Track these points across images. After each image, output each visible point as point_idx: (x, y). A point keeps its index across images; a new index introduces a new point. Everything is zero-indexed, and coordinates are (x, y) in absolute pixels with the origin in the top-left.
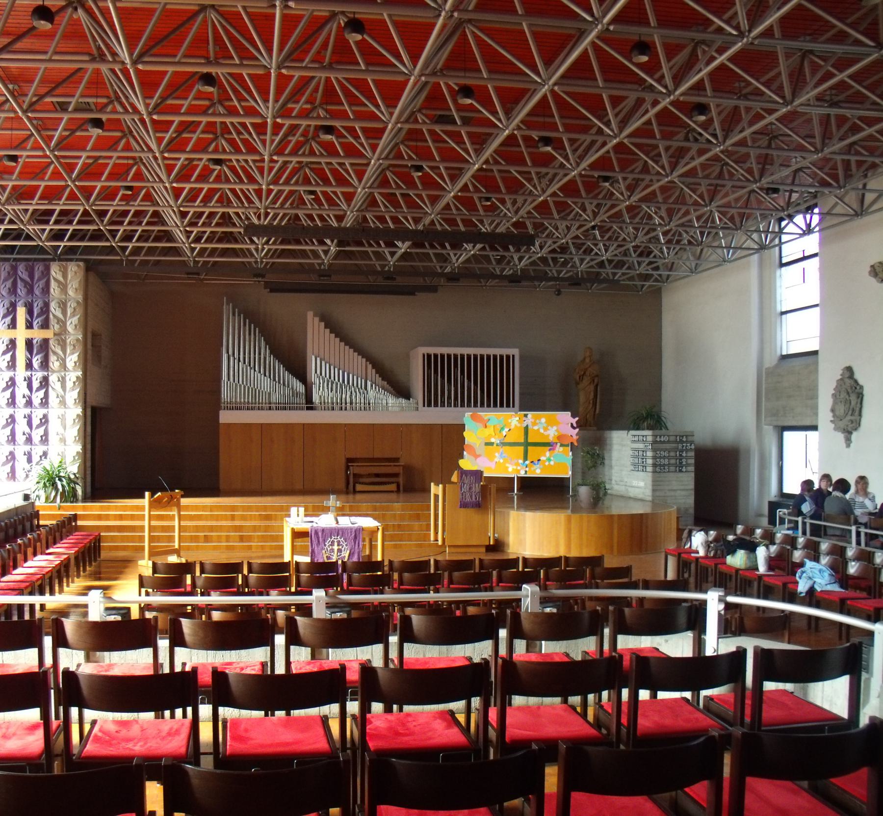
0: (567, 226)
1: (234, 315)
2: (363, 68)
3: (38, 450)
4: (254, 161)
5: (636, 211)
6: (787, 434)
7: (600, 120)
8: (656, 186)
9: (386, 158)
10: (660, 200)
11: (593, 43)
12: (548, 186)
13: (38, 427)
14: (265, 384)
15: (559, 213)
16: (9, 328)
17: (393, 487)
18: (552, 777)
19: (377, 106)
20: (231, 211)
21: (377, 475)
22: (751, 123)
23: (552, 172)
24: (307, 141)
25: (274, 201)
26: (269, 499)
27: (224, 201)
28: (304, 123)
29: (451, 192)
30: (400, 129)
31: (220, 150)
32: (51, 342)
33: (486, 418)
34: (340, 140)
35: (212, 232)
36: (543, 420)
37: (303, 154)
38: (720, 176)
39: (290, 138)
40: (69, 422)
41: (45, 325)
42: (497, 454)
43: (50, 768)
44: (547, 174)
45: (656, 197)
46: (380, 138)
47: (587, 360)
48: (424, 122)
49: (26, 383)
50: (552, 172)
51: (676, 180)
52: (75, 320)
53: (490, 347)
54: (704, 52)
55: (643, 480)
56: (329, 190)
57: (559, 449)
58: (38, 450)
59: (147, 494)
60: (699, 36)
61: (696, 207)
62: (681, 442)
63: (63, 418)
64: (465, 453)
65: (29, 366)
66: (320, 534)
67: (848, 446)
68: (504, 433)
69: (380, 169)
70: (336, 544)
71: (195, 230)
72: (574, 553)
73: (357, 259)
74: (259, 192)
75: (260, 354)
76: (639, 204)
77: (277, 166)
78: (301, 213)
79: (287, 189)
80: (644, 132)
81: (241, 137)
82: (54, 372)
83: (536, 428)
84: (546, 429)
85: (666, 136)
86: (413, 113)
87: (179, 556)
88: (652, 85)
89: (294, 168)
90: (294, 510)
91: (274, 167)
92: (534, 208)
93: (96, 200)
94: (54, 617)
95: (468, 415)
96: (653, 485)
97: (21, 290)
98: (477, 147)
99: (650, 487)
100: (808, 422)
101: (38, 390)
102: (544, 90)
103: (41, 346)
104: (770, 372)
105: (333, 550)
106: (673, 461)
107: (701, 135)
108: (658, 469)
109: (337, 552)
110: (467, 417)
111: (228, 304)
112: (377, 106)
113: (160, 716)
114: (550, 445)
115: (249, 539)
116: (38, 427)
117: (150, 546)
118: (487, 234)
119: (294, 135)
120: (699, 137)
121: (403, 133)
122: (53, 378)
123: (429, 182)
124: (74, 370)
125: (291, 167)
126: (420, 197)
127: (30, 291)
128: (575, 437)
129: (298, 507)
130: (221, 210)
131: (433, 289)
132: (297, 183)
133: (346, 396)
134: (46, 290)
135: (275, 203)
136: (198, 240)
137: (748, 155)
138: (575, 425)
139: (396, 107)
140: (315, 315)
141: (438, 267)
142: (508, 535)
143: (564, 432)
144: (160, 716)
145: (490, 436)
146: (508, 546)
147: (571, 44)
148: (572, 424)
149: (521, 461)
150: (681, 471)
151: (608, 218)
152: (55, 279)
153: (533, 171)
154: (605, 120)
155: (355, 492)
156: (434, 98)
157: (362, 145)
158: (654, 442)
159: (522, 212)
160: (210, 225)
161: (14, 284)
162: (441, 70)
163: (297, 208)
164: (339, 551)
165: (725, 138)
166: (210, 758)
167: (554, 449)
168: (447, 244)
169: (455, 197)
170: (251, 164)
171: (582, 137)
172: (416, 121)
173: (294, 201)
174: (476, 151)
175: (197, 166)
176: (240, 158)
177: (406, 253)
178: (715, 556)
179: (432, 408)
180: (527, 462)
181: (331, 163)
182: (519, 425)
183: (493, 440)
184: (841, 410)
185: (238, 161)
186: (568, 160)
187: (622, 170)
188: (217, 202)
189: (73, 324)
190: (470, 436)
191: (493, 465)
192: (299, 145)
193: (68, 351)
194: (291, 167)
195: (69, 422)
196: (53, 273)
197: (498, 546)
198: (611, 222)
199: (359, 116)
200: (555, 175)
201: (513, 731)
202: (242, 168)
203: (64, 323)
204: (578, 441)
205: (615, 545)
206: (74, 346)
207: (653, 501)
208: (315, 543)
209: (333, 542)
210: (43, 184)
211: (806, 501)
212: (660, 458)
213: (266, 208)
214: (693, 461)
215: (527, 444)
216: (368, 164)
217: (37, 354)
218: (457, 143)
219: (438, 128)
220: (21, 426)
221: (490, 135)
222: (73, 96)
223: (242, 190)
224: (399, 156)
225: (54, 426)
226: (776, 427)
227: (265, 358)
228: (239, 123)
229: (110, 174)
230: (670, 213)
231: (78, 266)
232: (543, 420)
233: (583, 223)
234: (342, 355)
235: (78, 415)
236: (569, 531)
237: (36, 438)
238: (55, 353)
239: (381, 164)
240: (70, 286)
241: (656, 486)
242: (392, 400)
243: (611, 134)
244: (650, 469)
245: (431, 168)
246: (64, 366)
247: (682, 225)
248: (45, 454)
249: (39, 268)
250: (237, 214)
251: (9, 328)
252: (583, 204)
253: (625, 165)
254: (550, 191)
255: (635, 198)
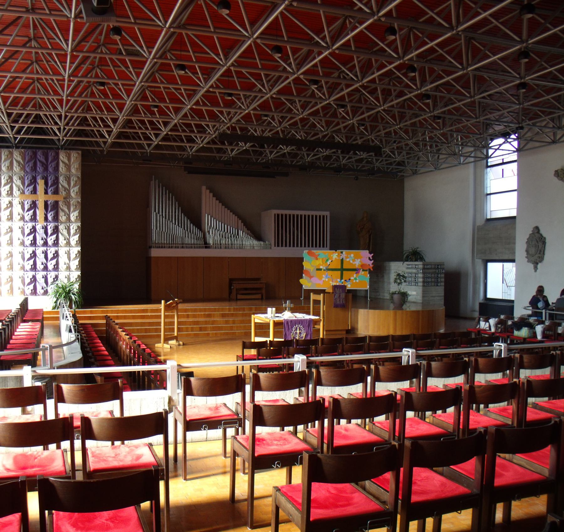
0: (262, 130)
1: (159, 187)
2: (133, 21)
3: (51, 275)
4: (58, 80)
5: (306, 122)
6: (490, 265)
7: (285, 63)
8: (319, 106)
9: (147, 81)
10: (322, 115)
11: (281, 13)
12: (251, 104)
13: (52, 259)
14: (179, 231)
15: (257, 121)
16: (32, 193)
17: (259, 296)
18: (33, 500)
19: (141, 47)
20: (41, 113)
21: (246, 289)
22: (379, 69)
23: (253, 94)
24: (93, 68)
25: (71, 108)
26: (205, 304)
27: (37, 106)
28: (92, 55)
29: (188, 106)
30: (156, 63)
31: (35, 72)
32: (60, 203)
33: (318, 254)
34: (116, 69)
35: (28, 127)
36: (352, 255)
37: (91, 77)
38: (359, 101)
39: (82, 66)
40: (73, 256)
41: (56, 192)
42: (324, 276)
43: (74, 476)
44: (250, 96)
45: (319, 113)
46: (143, 69)
47: (365, 219)
48: (172, 59)
49: (43, 230)
50: (253, 94)
51: (332, 103)
52: (76, 189)
53: (312, 210)
54: (350, 21)
55: (416, 291)
56: (107, 101)
57: (362, 272)
58: (51, 275)
59: (163, 302)
60: (347, 13)
61: (344, 120)
62: (438, 268)
63: (68, 254)
64: (304, 275)
65: (46, 219)
66: (289, 324)
67: (536, 271)
68: (328, 263)
69: (142, 89)
70: (298, 329)
71: (17, 126)
72: (398, 333)
73: (125, 148)
74: (61, 101)
75: (175, 212)
76: (308, 117)
77: (73, 84)
78: (88, 116)
79: (80, 100)
80: (312, 71)
81: (49, 63)
82: (62, 223)
83: (348, 260)
84: (354, 261)
85: (326, 75)
86: (164, 53)
87: (177, 340)
88: (318, 41)
89: (85, 86)
90: (269, 310)
91: (71, 85)
92: (241, 118)
93: (9, 105)
94: (254, 371)
95: (305, 252)
96: (423, 294)
97: (40, 169)
98: (206, 76)
99: (421, 295)
100: (511, 258)
101: (52, 235)
102: (249, 42)
103: (53, 205)
104: (480, 229)
105: (296, 333)
106: (433, 280)
107: (348, 75)
108: (425, 285)
109: (299, 334)
110: (305, 254)
111: (155, 180)
112: (141, 47)
113: (46, 448)
114: (356, 270)
115: (205, 329)
116: (52, 259)
117: (164, 335)
118: (258, 137)
119: (85, 64)
120: (346, 77)
121: (158, 65)
122: (61, 227)
123: (174, 99)
124: (76, 222)
125: (82, 85)
126: (168, 108)
127: (46, 169)
128: (371, 266)
129: (272, 308)
130: (35, 113)
131: (286, 174)
132: (86, 96)
133: (225, 238)
134: (57, 168)
135: (72, 109)
136: (18, 132)
137: (376, 89)
138: (371, 258)
139: (153, 48)
140: (207, 189)
141: (254, 159)
142: (357, 323)
143: (364, 263)
144: (46, 448)
145: (320, 265)
146: (357, 329)
147: (269, 11)
148: (369, 258)
149: (339, 280)
150: (437, 285)
151: (289, 125)
152: (40, 161)
153: (241, 93)
154: (288, 62)
155: (237, 300)
156: (177, 43)
157: (131, 72)
158: (424, 269)
159: (234, 120)
160: (27, 123)
161: (35, 164)
162: (184, 24)
163: (87, 113)
164: (300, 333)
165: (363, 78)
166: (81, 472)
167: (358, 273)
168: (226, 142)
169: (191, 109)
170: (56, 82)
171: (273, 74)
172: (166, 58)
173: (84, 108)
174: (204, 79)
175: (19, 82)
176: (48, 77)
177: (158, 144)
178: (500, 332)
179: (280, 248)
180: (343, 281)
181: (169, 88)
182: (338, 258)
183: (321, 267)
184: (532, 251)
185: (47, 80)
186: (264, 87)
187: (298, 95)
188: (32, 107)
189: (75, 191)
190: (306, 265)
191: (321, 282)
192: (89, 71)
193: (72, 210)
194: (82, 85)
195: (73, 256)
196: (61, 157)
197: (352, 331)
198: (290, 128)
199: (129, 53)
200: (256, 97)
201: (93, 465)
202: (49, 84)
203: (69, 191)
204: (373, 268)
205: (420, 328)
206: (76, 206)
207: (422, 303)
208: (287, 329)
209: (297, 328)
210: (12, 96)
211: (540, 301)
212: (427, 278)
213: (66, 112)
214: (443, 280)
215: (342, 270)
216: (134, 85)
217: (50, 211)
218: (193, 73)
219: (114, 57)
220: (40, 258)
221: (214, 69)
222: (11, 35)
223: (48, 99)
224: (154, 81)
225: (63, 259)
226: (483, 260)
227: (178, 216)
228: (47, 53)
229: (20, 88)
230: (328, 123)
231: (78, 153)
232: (352, 255)
233: (273, 128)
234: (223, 214)
235: (78, 251)
236: (395, 320)
237: (50, 267)
238: (63, 210)
239: (143, 85)
240: (72, 166)
241: (425, 294)
242: (255, 242)
243: (291, 71)
244: (421, 284)
245: (175, 89)
246: (69, 219)
247: (334, 131)
248: (57, 277)
249: (51, 155)
250: (46, 115)
251: (32, 193)
252: (273, 116)
253: (300, 92)
254: (252, 107)
255: (306, 113)
